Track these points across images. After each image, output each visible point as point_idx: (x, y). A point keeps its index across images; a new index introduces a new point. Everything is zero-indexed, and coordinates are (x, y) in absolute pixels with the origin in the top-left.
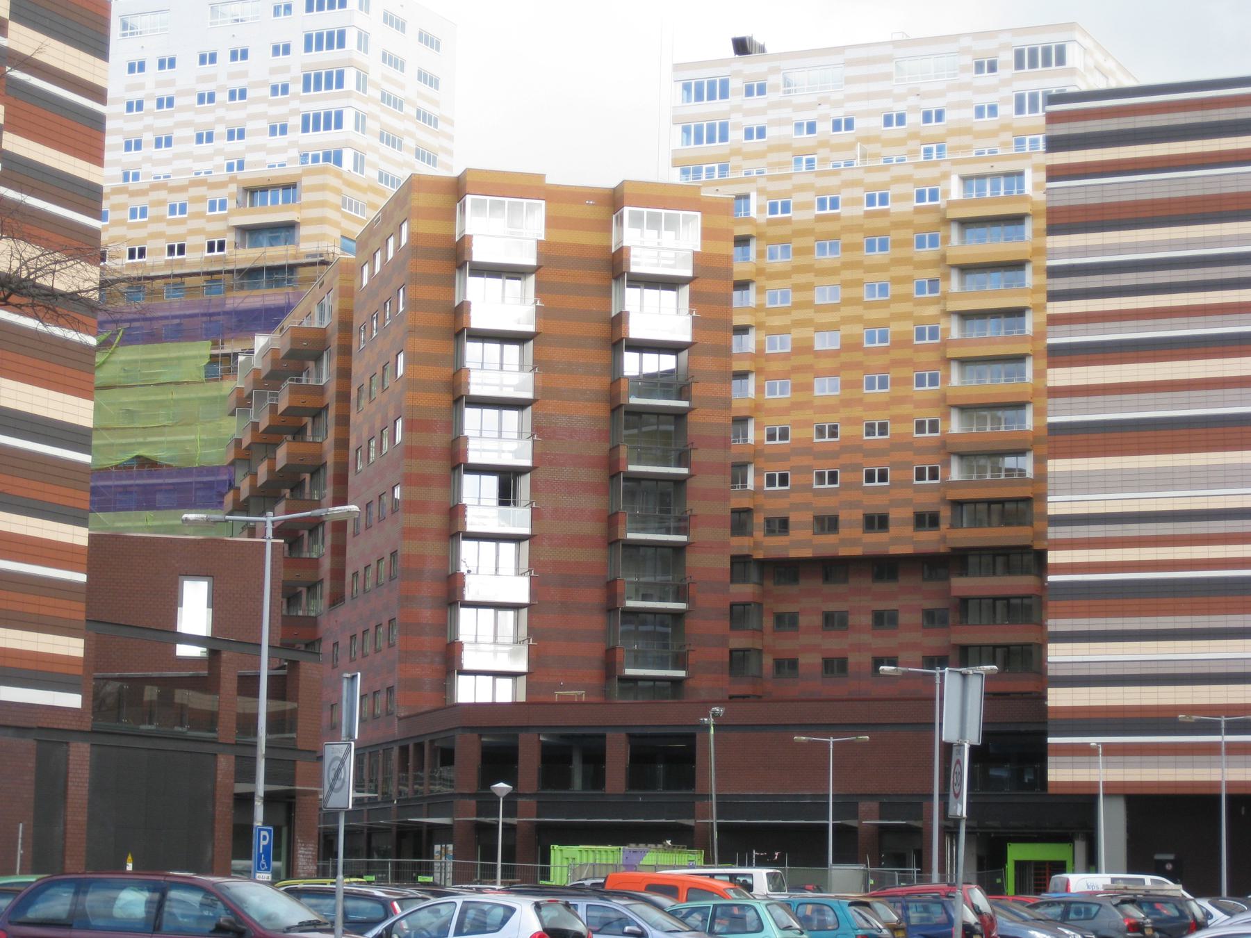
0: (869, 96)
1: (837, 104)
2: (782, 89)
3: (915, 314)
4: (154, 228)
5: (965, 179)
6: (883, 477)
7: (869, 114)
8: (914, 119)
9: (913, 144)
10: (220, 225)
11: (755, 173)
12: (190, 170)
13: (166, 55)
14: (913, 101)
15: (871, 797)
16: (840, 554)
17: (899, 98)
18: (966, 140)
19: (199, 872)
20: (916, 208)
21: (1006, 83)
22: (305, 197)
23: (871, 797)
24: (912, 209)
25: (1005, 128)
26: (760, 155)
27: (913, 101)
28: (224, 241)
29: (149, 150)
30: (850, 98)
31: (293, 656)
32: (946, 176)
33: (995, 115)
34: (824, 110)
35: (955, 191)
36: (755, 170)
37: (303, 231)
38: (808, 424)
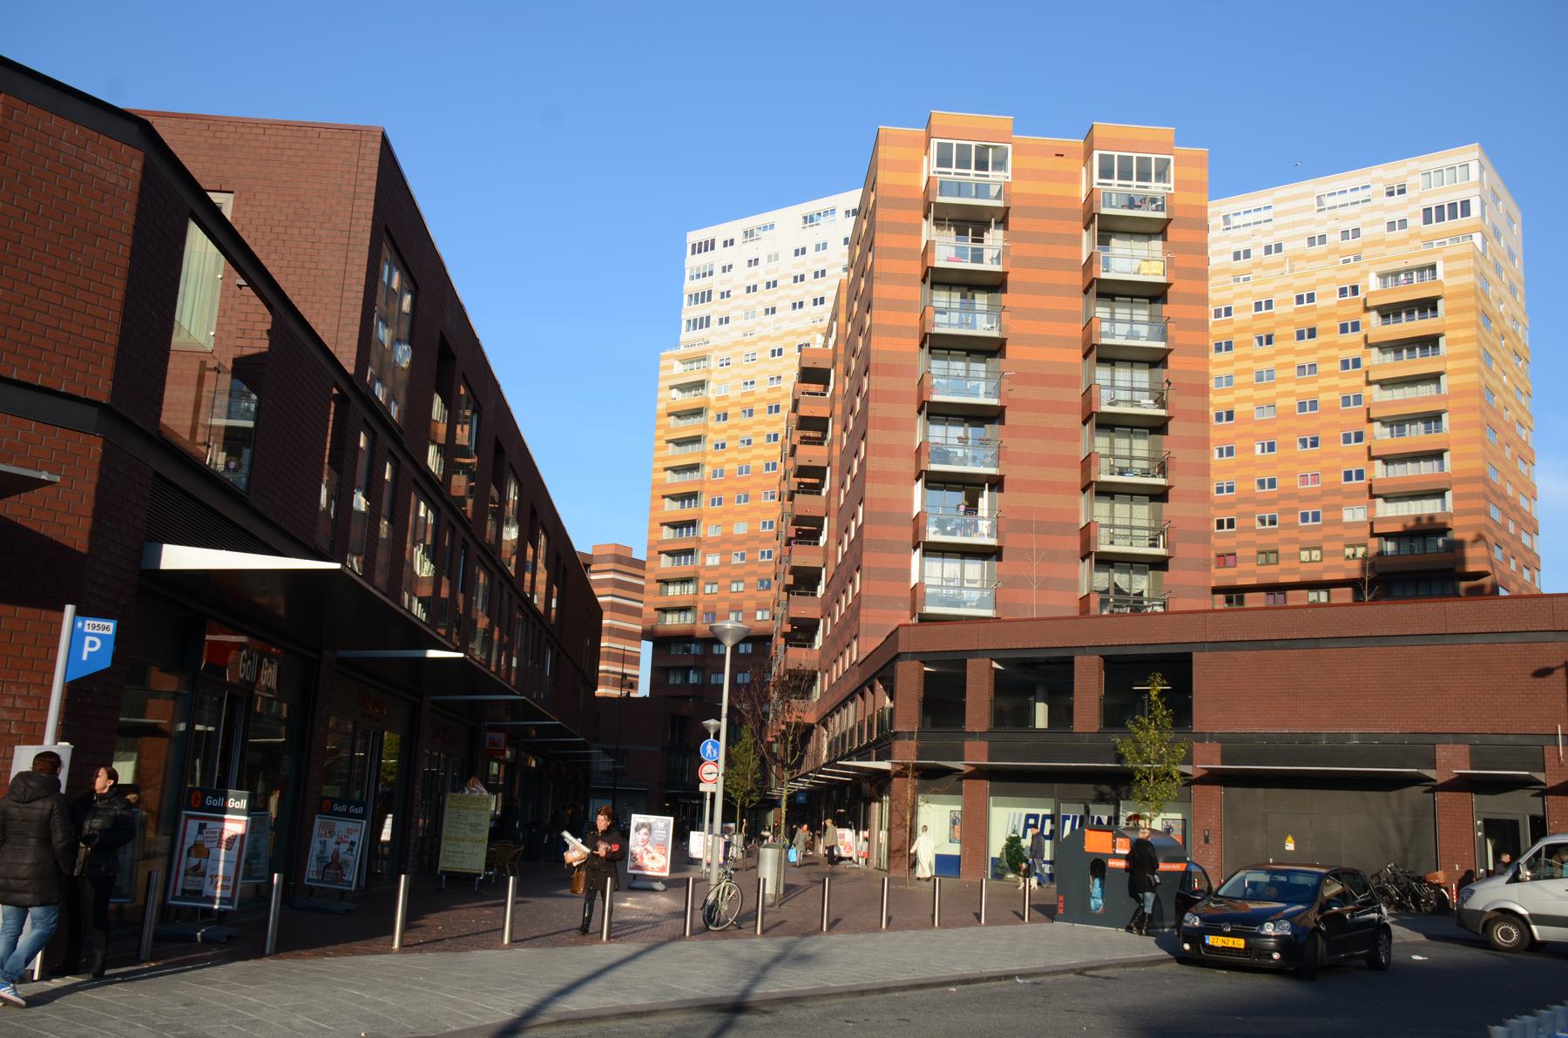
0: (1294, 225)
2: (1223, 227)
3: (1340, 386)
5: (1383, 276)
6: (1273, 522)
8: (1333, 238)
9: (1333, 258)
11: (1448, 242)
15: (1457, 737)
16: (1238, 584)
18: (1380, 249)
20: (1254, 316)
23: (1457, 737)
24: (1335, 303)
28: (1271, 301)
31: (323, 839)
32: (1365, 274)
33: (1249, 257)
35: (1373, 283)
36: (1448, 245)
38: (1250, 478)
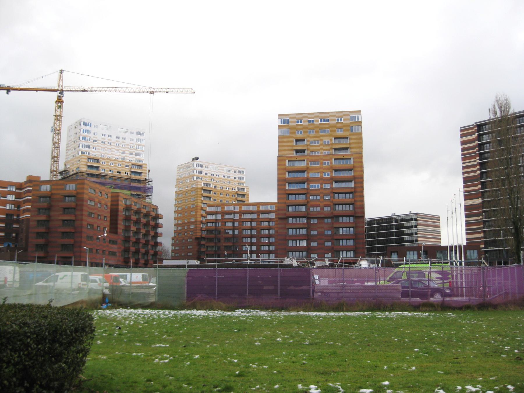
0: (221, 172)
1: (217, 172)
4: (115, 167)
7: (221, 175)
8: (226, 177)
10: (127, 170)
12: (114, 157)
13: (110, 134)
14: (226, 174)
17: (225, 173)
19: (84, 274)
21: (237, 175)
22: (143, 169)
25: (237, 181)
26: (218, 179)
27: (226, 174)
29: (91, 149)
30: (219, 172)
34: (215, 173)
37: (143, 174)
